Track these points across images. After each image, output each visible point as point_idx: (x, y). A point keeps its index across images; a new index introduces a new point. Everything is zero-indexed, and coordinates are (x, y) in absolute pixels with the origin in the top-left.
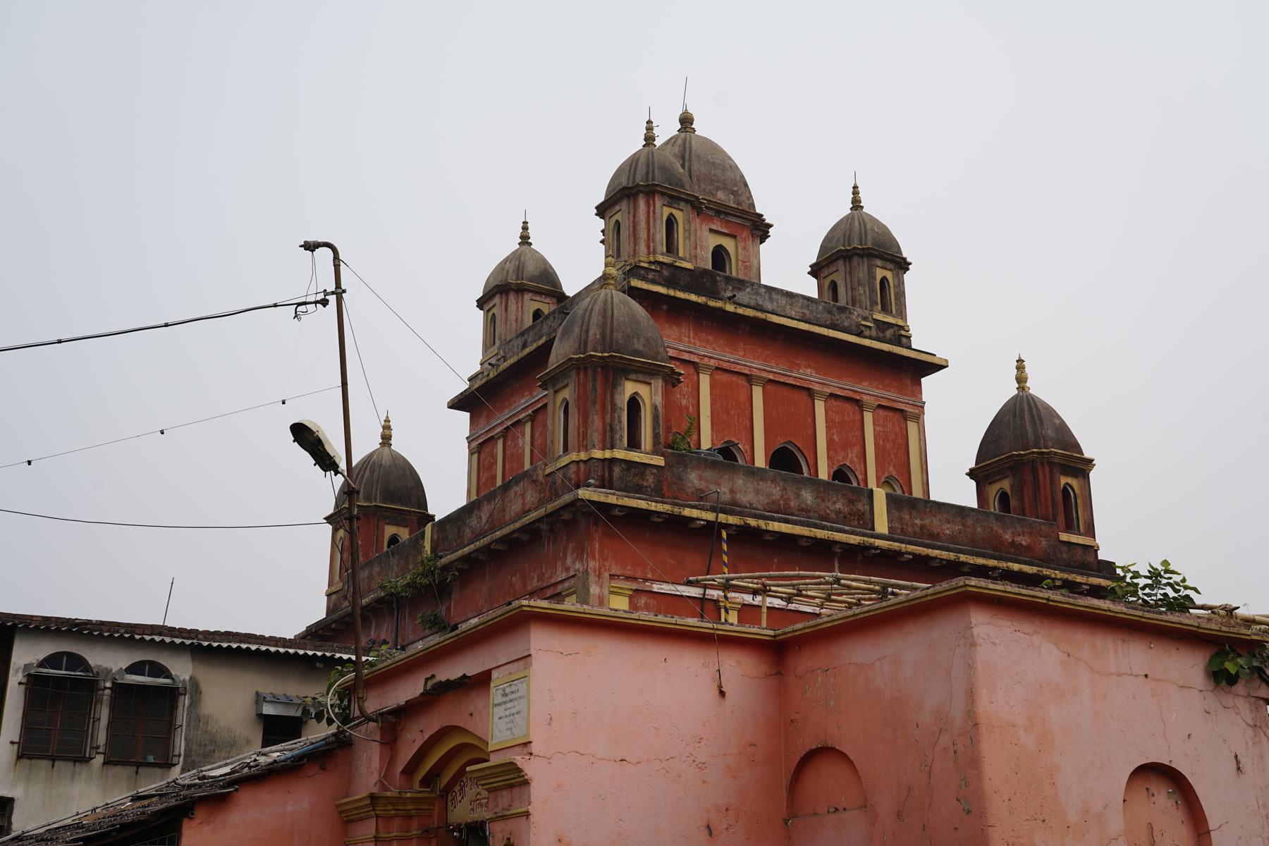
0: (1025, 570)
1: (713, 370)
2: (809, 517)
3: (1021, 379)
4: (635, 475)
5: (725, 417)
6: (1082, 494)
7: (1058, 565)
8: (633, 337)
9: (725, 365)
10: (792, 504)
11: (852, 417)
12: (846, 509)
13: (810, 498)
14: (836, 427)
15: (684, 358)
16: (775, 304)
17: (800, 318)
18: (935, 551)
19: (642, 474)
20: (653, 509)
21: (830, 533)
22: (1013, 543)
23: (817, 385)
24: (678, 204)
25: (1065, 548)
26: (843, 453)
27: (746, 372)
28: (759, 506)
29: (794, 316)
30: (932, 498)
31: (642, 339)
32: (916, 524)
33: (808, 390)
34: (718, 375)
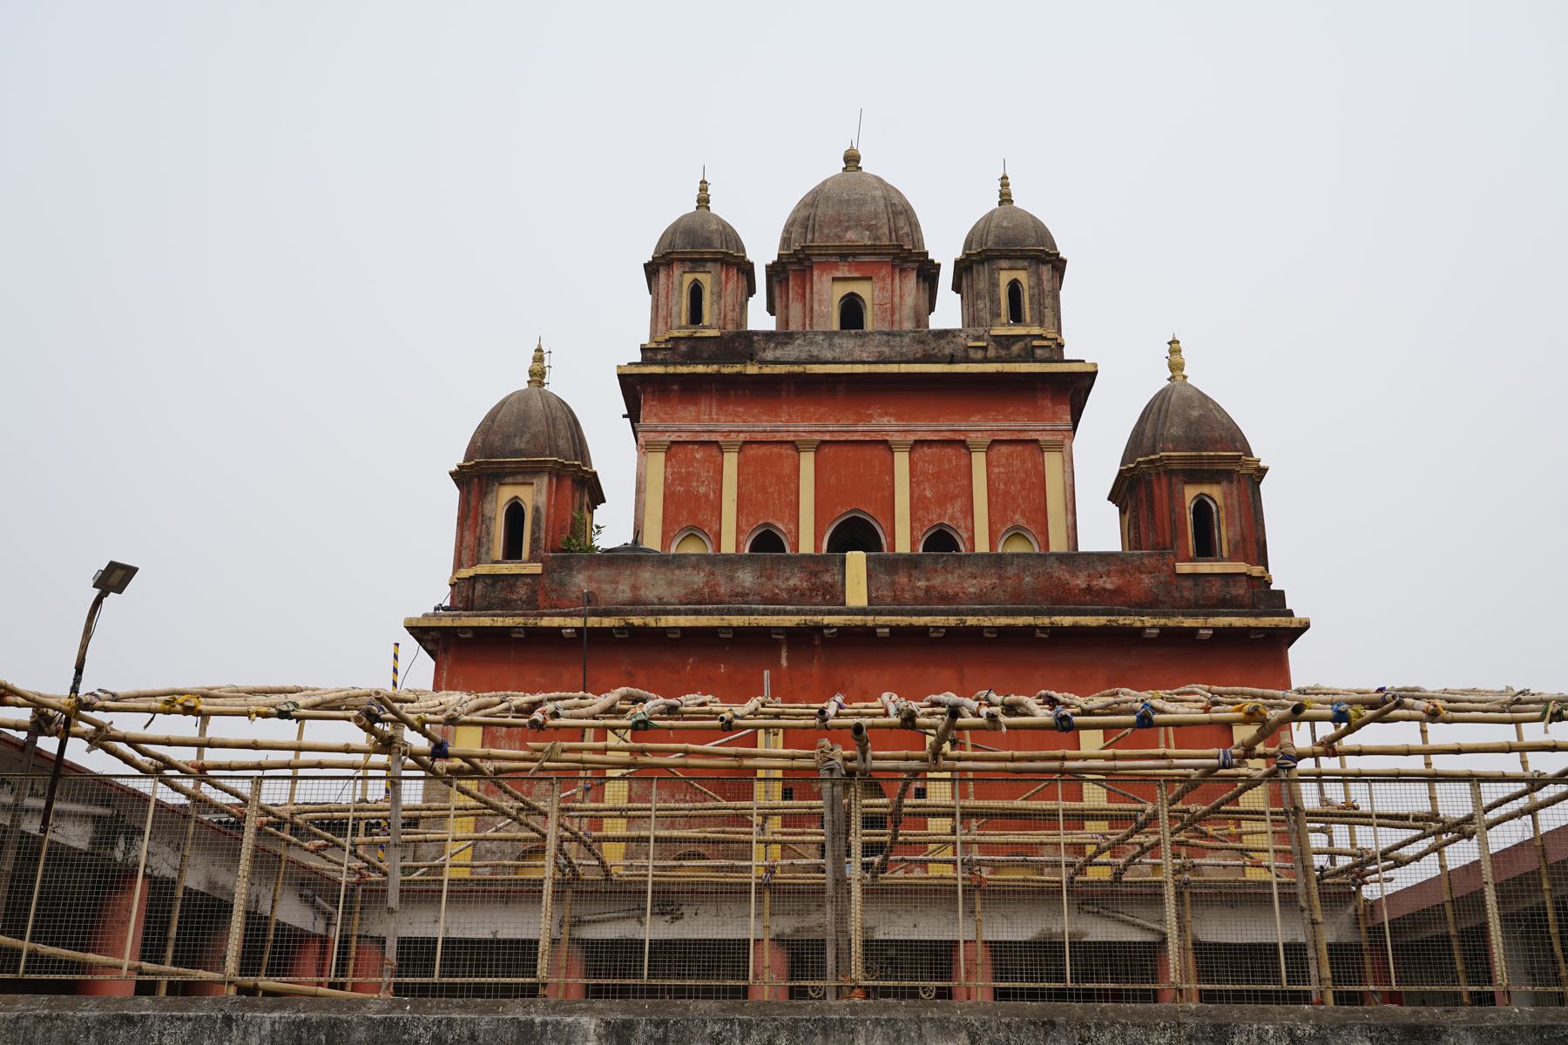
1: (669, 448)
3: (1176, 367)
6: (1226, 505)
9: (759, 437)
10: (722, 590)
12: (805, 584)
14: (928, 480)
15: (702, 439)
16: (838, 350)
19: (512, 588)
20: (500, 624)
22: (1089, 589)
25: (1189, 583)
26: (938, 510)
28: (672, 600)
30: (1082, 548)
31: (527, 436)
33: (885, 442)
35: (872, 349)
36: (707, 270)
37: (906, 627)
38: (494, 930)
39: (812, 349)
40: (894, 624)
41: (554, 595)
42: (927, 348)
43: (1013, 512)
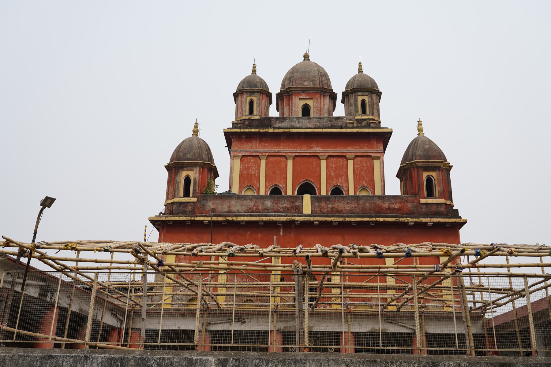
2: (268, 212)
3: (420, 130)
4: (183, 207)
7: (419, 215)
10: (260, 208)
11: (342, 164)
12: (289, 206)
15: (253, 155)
16: (301, 124)
17: (314, 127)
18: (330, 218)
21: (270, 217)
22: (389, 208)
23: (322, 153)
25: (424, 206)
26: (336, 180)
27: (284, 155)
28: (242, 211)
29: (311, 127)
32: (329, 207)
33: (318, 156)
34: (271, 158)
36: (255, 95)
39: (292, 123)
40: (320, 220)
41: (201, 209)
42: (332, 123)
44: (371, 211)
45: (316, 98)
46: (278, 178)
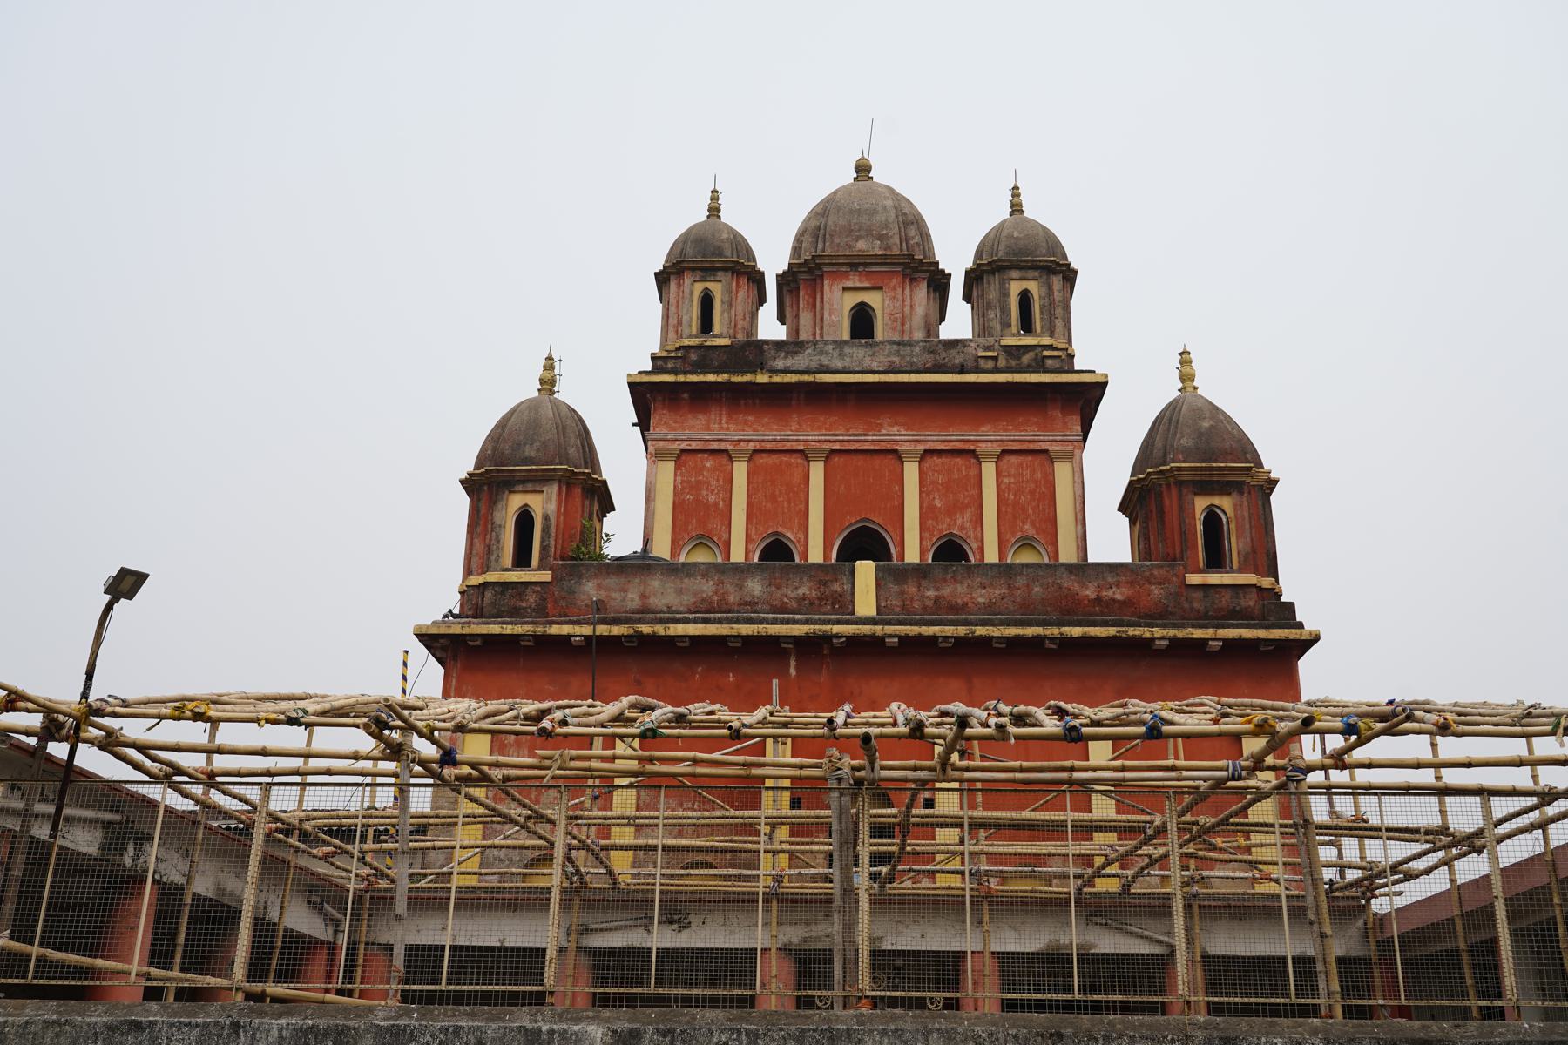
0: (1093, 634)
3: (1186, 378)
4: (512, 596)
5: (769, 505)
6: (1236, 516)
8: (525, 444)
10: (731, 599)
12: (814, 594)
13: (760, 588)
14: (938, 490)
15: (712, 448)
16: (848, 359)
19: (521, 596)
22: (1099, 600)
23: (908, 443)
24: (714, 275)
25: (1199, 595)
27: (801, 447)
33: (895, 452)
34: (762, 458)
35: (882, 358)
37: (915, 636)
38: (502, 938)
39: (822, 358)
41: (563, 603)
42: (937, 357)
43: (1023, 523)
44: (1049, 609)
45: (892, 284)
46: (783, 513)
